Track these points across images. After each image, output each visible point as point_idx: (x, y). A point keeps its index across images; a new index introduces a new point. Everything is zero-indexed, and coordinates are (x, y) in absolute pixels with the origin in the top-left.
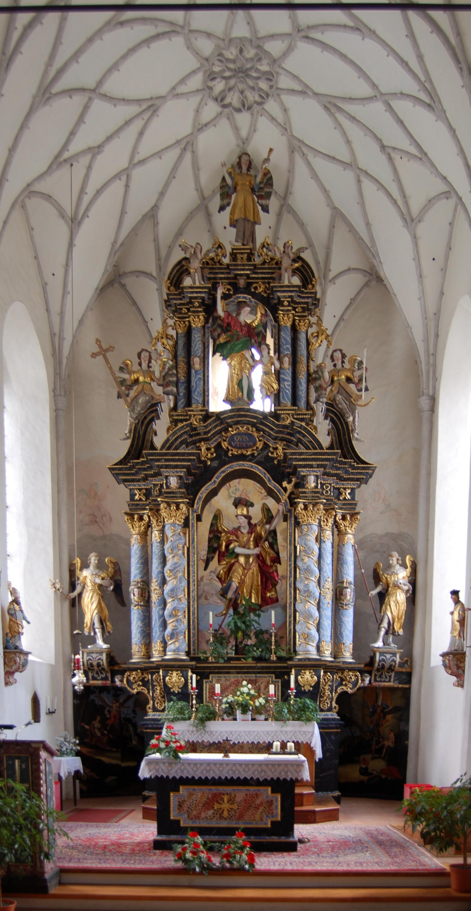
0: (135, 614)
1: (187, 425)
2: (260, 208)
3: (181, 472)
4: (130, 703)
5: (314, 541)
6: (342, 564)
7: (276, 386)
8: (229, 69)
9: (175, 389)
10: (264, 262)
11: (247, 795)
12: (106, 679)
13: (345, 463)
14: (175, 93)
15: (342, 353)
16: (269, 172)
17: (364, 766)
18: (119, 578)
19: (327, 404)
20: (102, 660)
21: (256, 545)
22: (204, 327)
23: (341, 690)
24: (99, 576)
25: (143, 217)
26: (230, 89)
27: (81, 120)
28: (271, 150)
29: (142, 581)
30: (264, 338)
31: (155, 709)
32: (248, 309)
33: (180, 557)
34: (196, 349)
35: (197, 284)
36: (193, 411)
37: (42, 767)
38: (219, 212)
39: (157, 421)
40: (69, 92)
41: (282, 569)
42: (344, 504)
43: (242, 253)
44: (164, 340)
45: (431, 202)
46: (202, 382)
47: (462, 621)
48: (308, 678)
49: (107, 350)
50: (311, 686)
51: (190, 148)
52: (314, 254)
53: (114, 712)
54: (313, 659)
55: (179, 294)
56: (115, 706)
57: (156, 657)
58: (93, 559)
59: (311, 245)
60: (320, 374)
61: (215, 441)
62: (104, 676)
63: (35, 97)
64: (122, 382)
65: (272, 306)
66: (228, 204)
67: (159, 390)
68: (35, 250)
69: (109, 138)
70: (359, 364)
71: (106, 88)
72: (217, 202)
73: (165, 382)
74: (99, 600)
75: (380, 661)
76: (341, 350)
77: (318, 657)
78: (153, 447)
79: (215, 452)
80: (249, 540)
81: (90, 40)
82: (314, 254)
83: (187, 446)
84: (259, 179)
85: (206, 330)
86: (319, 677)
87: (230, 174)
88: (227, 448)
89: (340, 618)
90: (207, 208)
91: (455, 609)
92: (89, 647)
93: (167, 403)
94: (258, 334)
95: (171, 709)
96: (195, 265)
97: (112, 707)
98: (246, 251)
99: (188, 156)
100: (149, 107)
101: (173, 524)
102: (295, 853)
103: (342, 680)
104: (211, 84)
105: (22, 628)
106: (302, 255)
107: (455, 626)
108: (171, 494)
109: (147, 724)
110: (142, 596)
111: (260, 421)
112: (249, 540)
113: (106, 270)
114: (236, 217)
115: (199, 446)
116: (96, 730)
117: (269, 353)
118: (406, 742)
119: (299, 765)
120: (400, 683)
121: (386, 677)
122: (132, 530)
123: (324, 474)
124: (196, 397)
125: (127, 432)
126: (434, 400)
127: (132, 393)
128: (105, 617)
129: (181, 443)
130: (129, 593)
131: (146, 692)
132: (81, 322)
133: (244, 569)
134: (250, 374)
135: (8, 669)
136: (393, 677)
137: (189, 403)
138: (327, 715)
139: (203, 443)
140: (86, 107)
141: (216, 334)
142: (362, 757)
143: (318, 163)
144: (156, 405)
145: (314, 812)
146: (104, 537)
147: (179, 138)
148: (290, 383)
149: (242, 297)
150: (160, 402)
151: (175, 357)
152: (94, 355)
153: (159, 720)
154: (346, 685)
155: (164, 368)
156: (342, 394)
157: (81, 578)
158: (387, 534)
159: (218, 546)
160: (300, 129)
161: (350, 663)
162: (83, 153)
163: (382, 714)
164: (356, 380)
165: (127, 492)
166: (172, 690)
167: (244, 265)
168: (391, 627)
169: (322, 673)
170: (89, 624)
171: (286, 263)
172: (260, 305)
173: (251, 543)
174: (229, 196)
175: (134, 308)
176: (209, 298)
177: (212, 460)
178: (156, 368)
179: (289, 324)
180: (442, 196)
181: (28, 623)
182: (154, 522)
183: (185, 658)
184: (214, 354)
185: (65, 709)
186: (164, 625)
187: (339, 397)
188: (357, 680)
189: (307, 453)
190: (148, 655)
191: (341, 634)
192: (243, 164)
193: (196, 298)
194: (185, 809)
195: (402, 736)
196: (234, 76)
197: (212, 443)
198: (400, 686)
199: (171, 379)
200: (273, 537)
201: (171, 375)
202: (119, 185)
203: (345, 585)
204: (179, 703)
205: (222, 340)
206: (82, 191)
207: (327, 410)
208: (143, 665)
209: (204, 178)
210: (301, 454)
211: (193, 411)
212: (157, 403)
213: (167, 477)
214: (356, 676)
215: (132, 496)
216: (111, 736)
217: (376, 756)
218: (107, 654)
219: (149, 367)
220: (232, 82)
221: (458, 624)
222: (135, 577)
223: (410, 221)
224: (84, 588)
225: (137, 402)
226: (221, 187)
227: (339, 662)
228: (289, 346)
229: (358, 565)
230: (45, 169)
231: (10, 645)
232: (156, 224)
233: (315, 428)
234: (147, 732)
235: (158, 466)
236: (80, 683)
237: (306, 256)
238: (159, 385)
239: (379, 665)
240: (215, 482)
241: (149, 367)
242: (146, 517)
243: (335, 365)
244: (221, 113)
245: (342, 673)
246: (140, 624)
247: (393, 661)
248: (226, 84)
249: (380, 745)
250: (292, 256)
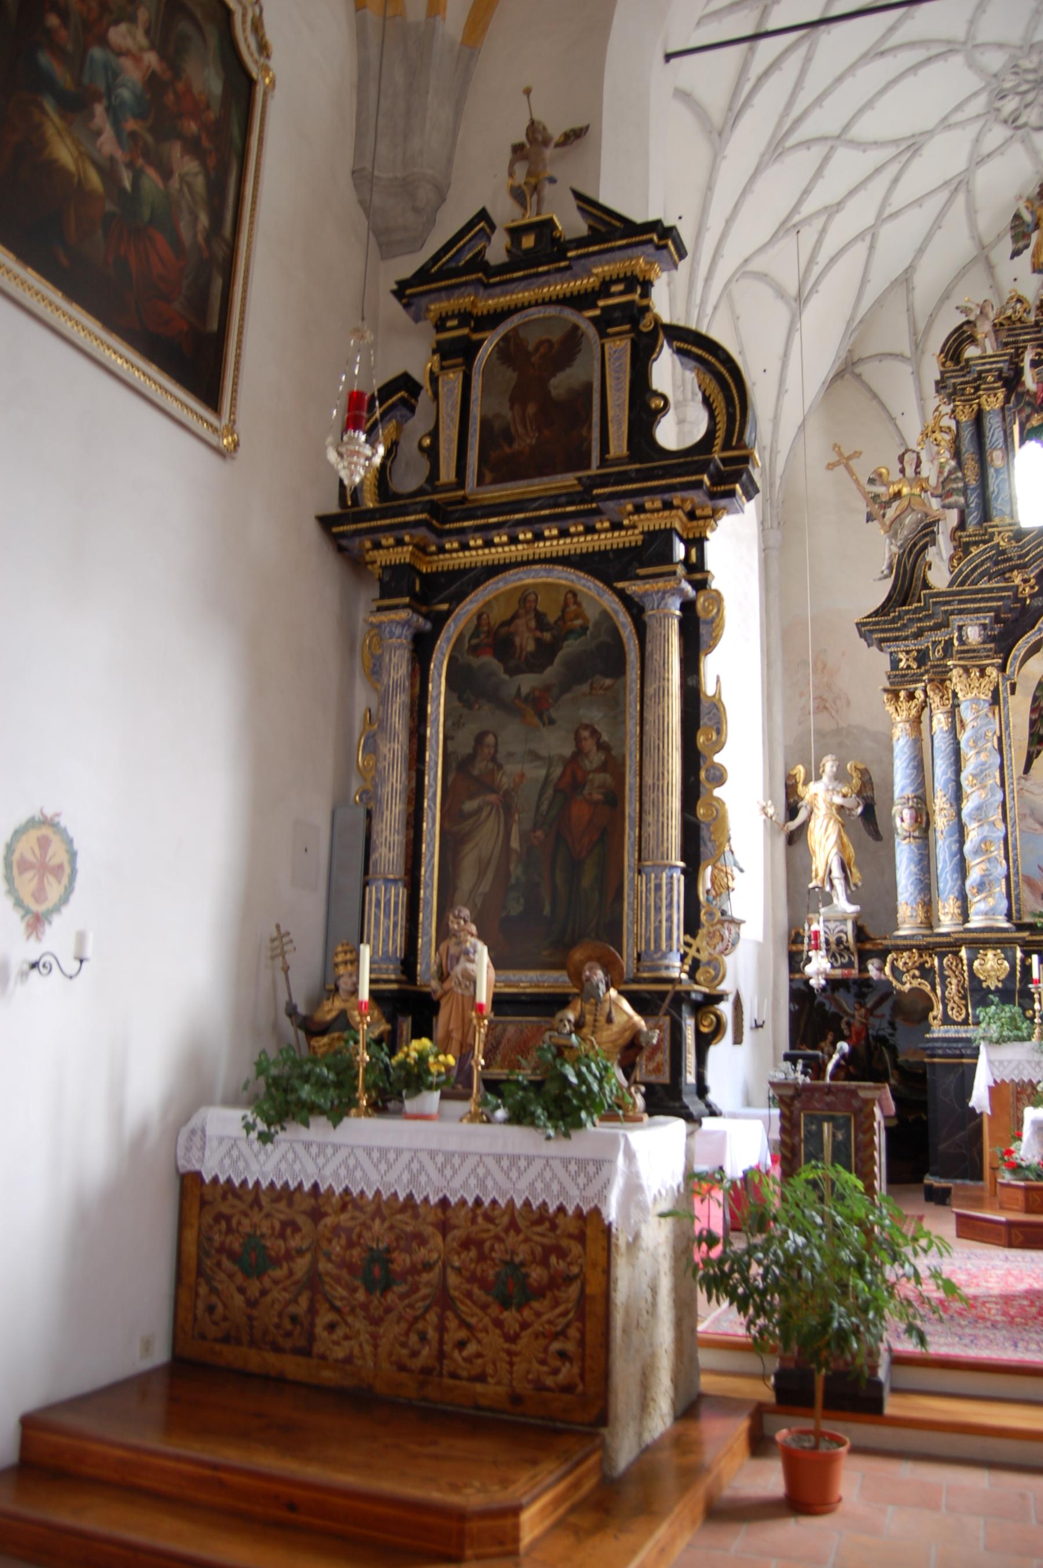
0: (904, 854)
1: (992, 548)
3: (985, 618)
4: (885, 1009)
8: (1027, 82)
12: (850, 965)
14: (945, 124)
18: (869, 793)
20: (846, 934)
22: (1003, 409)
24: (838, 792)
26: (1027, 106)
29: (915, 797)
31: (947, 1020)
33: (990, 752)
34: (994, 439)
35: (990, 352)
36: (996, 526)
38: (1012, 257)
40: (807, 144)
49: (849, 458)
51: (963, 187)
53: (857, 1024)
56: (859, 1014)
57: (947, 922)
58: (829, 765)
61: (1036, 568)
62: (846, 960)
63: (763, 155)
64: (876, 497)
66: (1027, 246)
67: (935, 504)
69: (852, 193)
71: (857, 132)
72: (1008, 245)
79: (1036, 584)
81: (839, 79)
83: (989, 580)
85: (1007, 413)
90: (987, 258)
93: (952, 518)
95: (993, 1019)
97: (853, 1016)
100: (910, 146)
101: (976, 700)
105: (733, 879)
108: (968, 653)
109: (933, 1048)
110: (916, 821)
113: (837, 357)
115: (1010, 578)
122: (895, 715)
124: (997, 505)
125: (884, 568)
128: (849, 859)
129: (982, 575)
130: (891, 818)
132: (802, 427)
137: (986, 516)
139: (1015, 572)
140: (826, 159)
146: (838, 731)
147: (948, 177)
150: (939, 520)
151: (957, 454)
153: (968, 1040)
157: (807, 797)
162: (818, 213)
165: (883, 661)
166: (984, 985)
170: (821, 874)
174: (1026, 236)
175: (874, 402)
176: (1009, 369)
177: (1032, 596)
178: (929, 470)
181: (741, 871)
182: (935, 700)
183: (1006, 925)
186: (962, 869)
190: (929, 921)
193: (990, 371)
196: (1034, 88)
197: (1032, 571)
199: (954, 486)
204: (1007, 1009)
206: (812, 260)
208: (923, 942)
209: (983, 221)
211: (996, 526)
213: (960, 628)
215: (895, 663)
216: (851, 1068)
219: (917, 473)
220: (1030, 97)
222: (902, 790)
224: (811, 812)
226: (1012, 228)
230: (767, 239)
232: (910, 290)
234: (933, 1064)
235: (946, 612)
236: (818, 974)
241: (917, 473)
242: (919, 695)
246: (913, 868)
248: (1022, 99)
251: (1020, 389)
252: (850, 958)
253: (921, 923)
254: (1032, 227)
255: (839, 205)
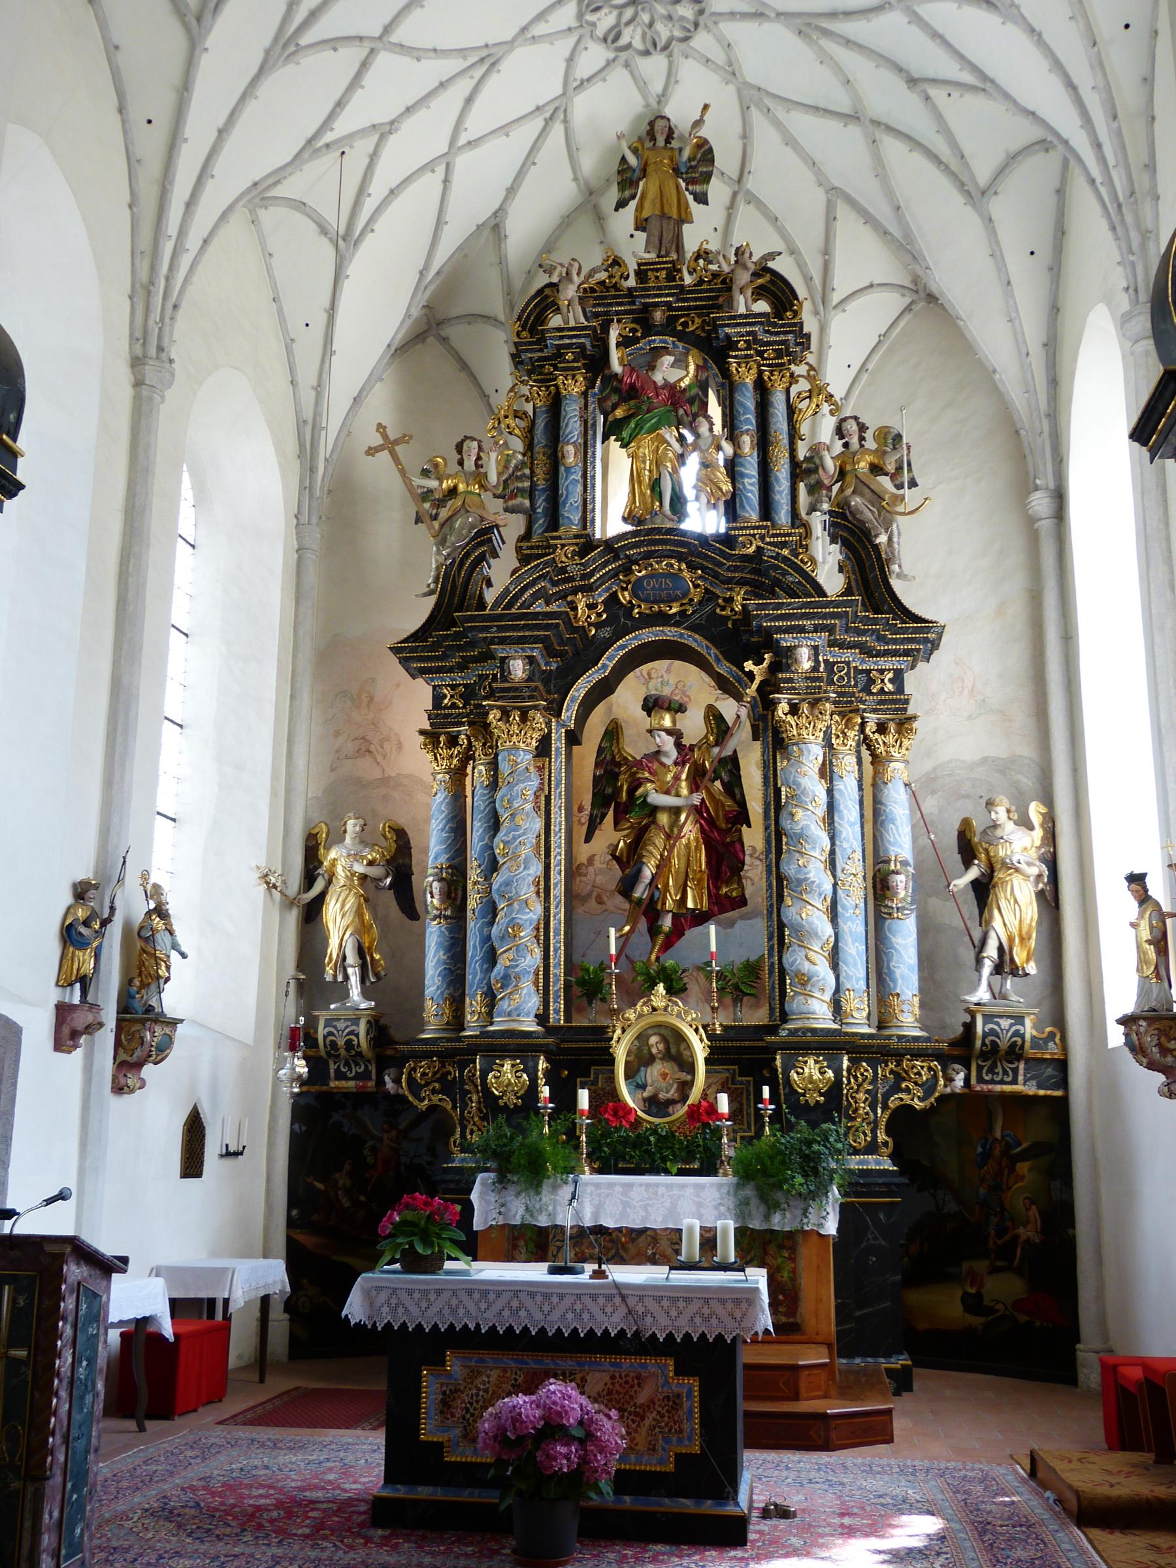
2: (690, 198)
5: (817, 777)
6: (883, 823)
7: (727, 487)
9: (527, 502)
10: (701, 282)
11: (613, 1377)
12: (365, 1076)
13: (875, 622)
15: (858, 424)
16: (706, 142)
17: (973, 1291)
19: (830, 513)
20: (357, 1035)
21: (694, 787)
22: (585, 394)
23: (898, 1103)
25: (478, 227)
27: (356, 82)
28: (706, 107)
30: (704, 405)
32: (668, 359)
34: (568, 430)
35: (572, 323)
36: (559, 538)
37: (68, 1305)
38: (616, 209)
39: (492, 561)
40: (333, 43)
41: (753, 837)
42: (881, 702)
43: (657, 270)
44: (509, 421)
45: (1013, 158)
46: (580, 488)
47: (1160, 943)
48: (811, 1073)
49: (396, 442)
50: (821, 1095)
52: (801, 266)
54: (822, 1030)
55: (538, 342)
59: (793, 251)
60: (817, 461)
63: (268, 52)
64: (427, 494)
65: (716, 352)
66: (633, 197)
67: (494, 508)
68: (274, 287)
70: (894, 440)
72: (613, 194)
73: (508, 491)
74: (359, 907)
75: (985, 1035)
76: (856, 418)
77: (836, 1026)
78: (482, 605)
80: (677, 778)
82: (801, 266)
84: (686, 154)
85: (590, 399)
86: (838, 1072)
87: (635, 151)
88: (630, 602)
89: (886, 937)
91: (1141, 915)
92: (332, 1006)
93: (513, 527)
94: (691, 402)
96: (570, 292)
97: (381, 1140)
98: (665, 265)
99: (558, 129)
100: (482, 60)
102: (739, 1553)
103: (899, 1078)
104: (590, 17)
106: (770, 264)
107: (1145, 953)
111: (696, 551)
112: (677, 778)
113: (408, 315)
114: (645, 214)
115: (572, 602)
116: (340, 1193)
117: (711, 430)
118: (1070, 1231)
119: (745, 1298)
120: (1039, 1087)
121: (1005, 1073)
123: (832, 644)
125: (430, 581)
126: (1060, 497)
127: (444, 513)
129: (535, 597)
131: (449, 1107)
133: (668, 837)
134: (675, 471)
135: (123, 1056)
136: (1021, 1072)
138: (867, 1163)
139: (580, 595)
140: (364, 65)
141: (609, 403)
142: (965, 1266)
143: (799, 122)
144: (489, 530)
145: (824, 1417)
148: (755, 480)
149: (657, 340)
151: (530, 447)
152: (371, 451)
154: (908, 1090)
155: (506, 467)
156: (862, 495)
158: (985, 760)
159: (616, 789)
160: (753, 69)
161: (916, 1039)
162: (362, 133)
163: (1004, 1162)
164: (891, 468)
165: (429, 690)
167: (660, 288)
168: (1007, 958)
169: (846, 1064)
170: (334, 956)
171: (743, 278)
172: (695, 351)
173: (684, 784)
174: (634, 184)
175: (463, 375)
176: (593, 346)
177: (598, 626)
179: (749, 380)
180: (1037, 147)
181: (184, 956)
184: (605, 438)
185: (271, 1145)
187: (856, 501)
188: (935, 1077)
189: (791, 603)
190: (457, 1022)
191: (891, 973)
192: (655, 132)
193: (569, 346)
194: (459, 1413)
195: (1060, 1215)
197: (600, 595)
198: (1042, 1092)
199: (520, 485)
200: (730, 771)
201: (520, 479)
202: (433, 181)
203: (892, 867)
205: (619, 413)
207: (833, 524)
210: (779, 606)
212: (491, 528)
213: (503, 660)
214: (930, 1069)
215: (437, 699)
217: (999, 1263)
218: (369, 1022)
221: (1151, 951)
222: (436, 858)
223: (976, 195)
224: (330, 882)
225: (452, 528)
226: (619, 172)
227: (889, 1037)
228: (751, 417)
229: (922, 824)
231: (137, 1004)
233: (813, 561)
237: (783, 266)
238: (495, 496)
239: (984, 1044)
240: (604, 666)
241: (477, 466)
243: (846, 445)
244: (614, 60)
245: (899, 1064)
247: (1017, 1033)
249: (1007, 1237)
250: (752, 267)
251: (607, 372)
252: (366, 1067)
253: (448, 1023)
254: (637, 174)
255: (392, 126)
